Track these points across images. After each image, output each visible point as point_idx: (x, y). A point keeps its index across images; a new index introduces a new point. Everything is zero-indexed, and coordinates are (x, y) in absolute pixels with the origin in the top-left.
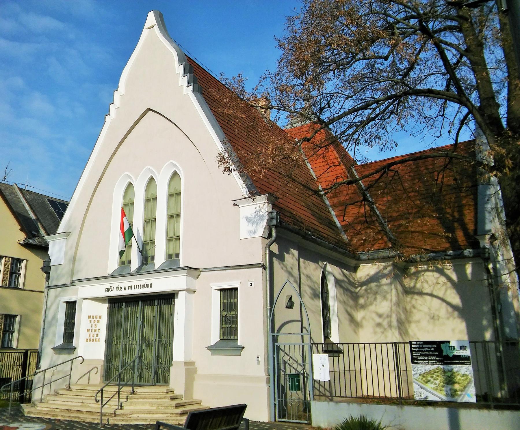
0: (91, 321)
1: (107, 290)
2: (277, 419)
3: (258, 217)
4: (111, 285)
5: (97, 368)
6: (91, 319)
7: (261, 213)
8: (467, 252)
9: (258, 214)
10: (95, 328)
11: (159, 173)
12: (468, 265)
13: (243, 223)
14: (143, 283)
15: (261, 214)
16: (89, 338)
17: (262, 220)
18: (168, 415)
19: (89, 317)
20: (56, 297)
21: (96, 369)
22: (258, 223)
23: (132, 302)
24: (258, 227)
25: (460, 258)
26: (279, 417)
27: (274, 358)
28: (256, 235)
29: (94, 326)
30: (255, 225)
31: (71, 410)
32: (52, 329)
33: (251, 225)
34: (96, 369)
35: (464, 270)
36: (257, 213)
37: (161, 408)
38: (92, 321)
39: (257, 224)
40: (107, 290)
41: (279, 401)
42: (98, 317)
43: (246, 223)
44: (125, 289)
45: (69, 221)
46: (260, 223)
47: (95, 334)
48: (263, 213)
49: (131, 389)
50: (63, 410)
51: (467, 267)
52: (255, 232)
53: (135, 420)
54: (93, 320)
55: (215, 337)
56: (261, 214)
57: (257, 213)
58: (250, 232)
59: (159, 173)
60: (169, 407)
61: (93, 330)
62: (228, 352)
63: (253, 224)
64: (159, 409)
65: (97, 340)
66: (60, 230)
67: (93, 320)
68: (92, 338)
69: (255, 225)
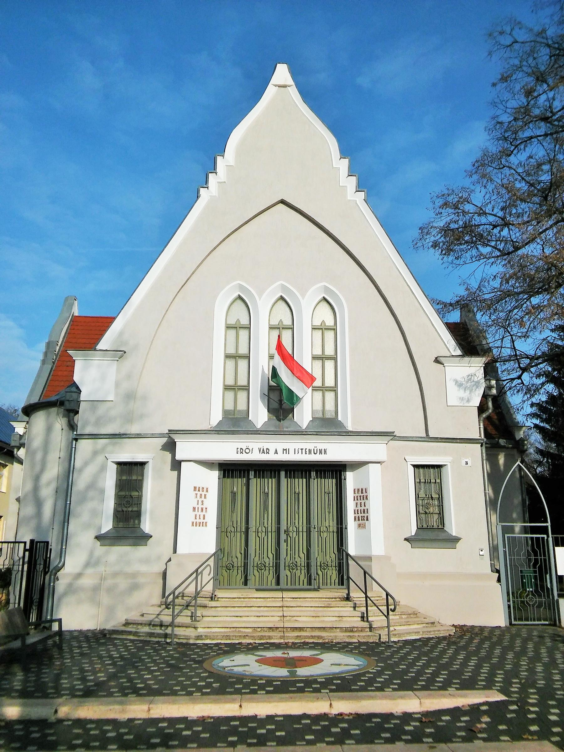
0: (196, 494)
1: (242, 451)
2: (513, 622)
3: (471, 382)
4: (248, 444)
5: (210, 567)
6: (197, 492)
7: (476, 378)
8: (502, 442)
9: (472, 378)
10: (202, 506)
11: (303, 299)
12: (501, 455)
13: (451, 387)
14: (311, 446)
15: (476, 380)
16: (195, 521)
17: (477, 387)
18: (424, 625)
19: (195, 488)
20: (95, 453)
21: (209, 567)
22: (472, 389)
23: (236, 470)
24: (473, 394)
25: (497, 448)
26: (515, 619)
27: (505, 552)
28: (471, 404)
29: (200, 502)
30: (468, 392)
31: (277, 628)
32: (90, 505)
33: (462, 391)
34: (209, 567)
35: (498, 461)
36: (470, 377)
37: (403, 616)
38: (198, 496)
39: (471, 391)
40: (242, 451)
41: (514, 602)
42: (205, 490)
43: (456, 388)
44: (276, 452)
45: (121, 334)
46: (476, 390)
47: (202, 514)
48: (479, 379)
49: (198, 602)
50: (259, 630)
51: (499, 457)
52: (468, 401)
53: (407, 633)
54: (199, 493)
55: (107, 526)
56: (476, 379)
57: (470, 377)
58: (462, 399)
59: (303, 299)
60: (412, 616)
61: (200, 509)
62: (426, 544)
63: (465, 390)
64: (402, 618)
65: (204, 525)
66: (103, 344)
67: (199, 493)
68: (198, 520)
69: (468, 392)
